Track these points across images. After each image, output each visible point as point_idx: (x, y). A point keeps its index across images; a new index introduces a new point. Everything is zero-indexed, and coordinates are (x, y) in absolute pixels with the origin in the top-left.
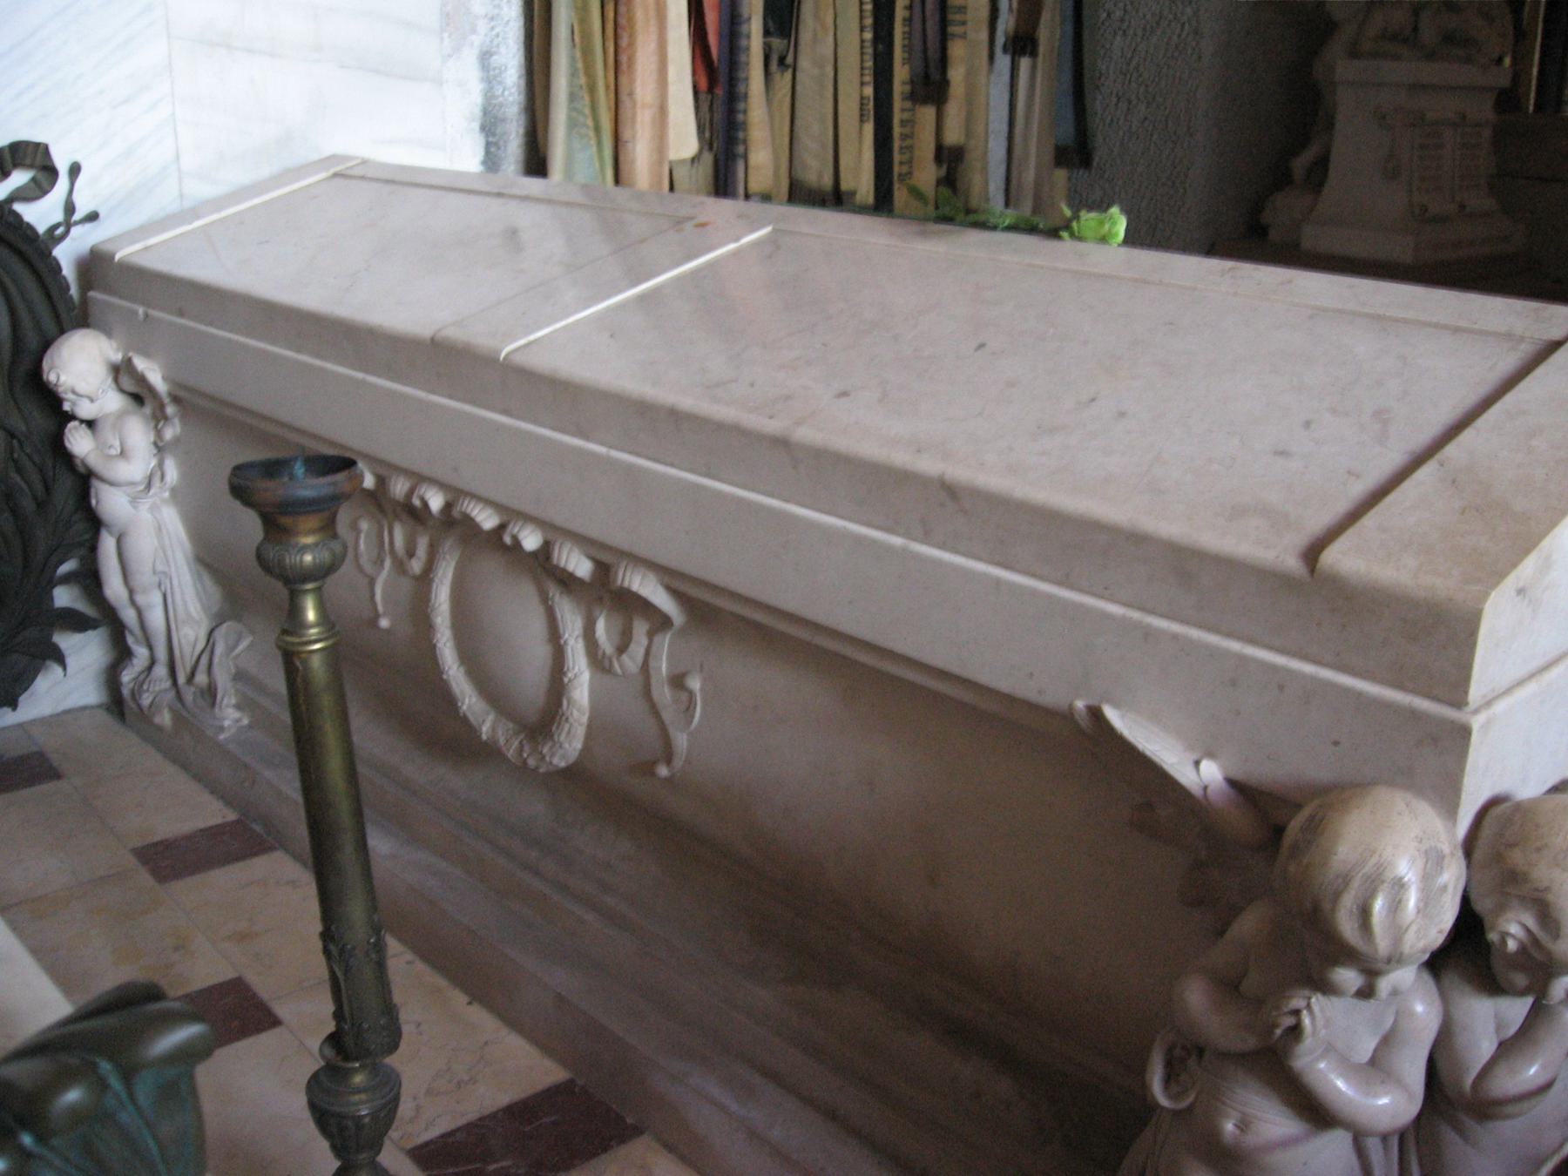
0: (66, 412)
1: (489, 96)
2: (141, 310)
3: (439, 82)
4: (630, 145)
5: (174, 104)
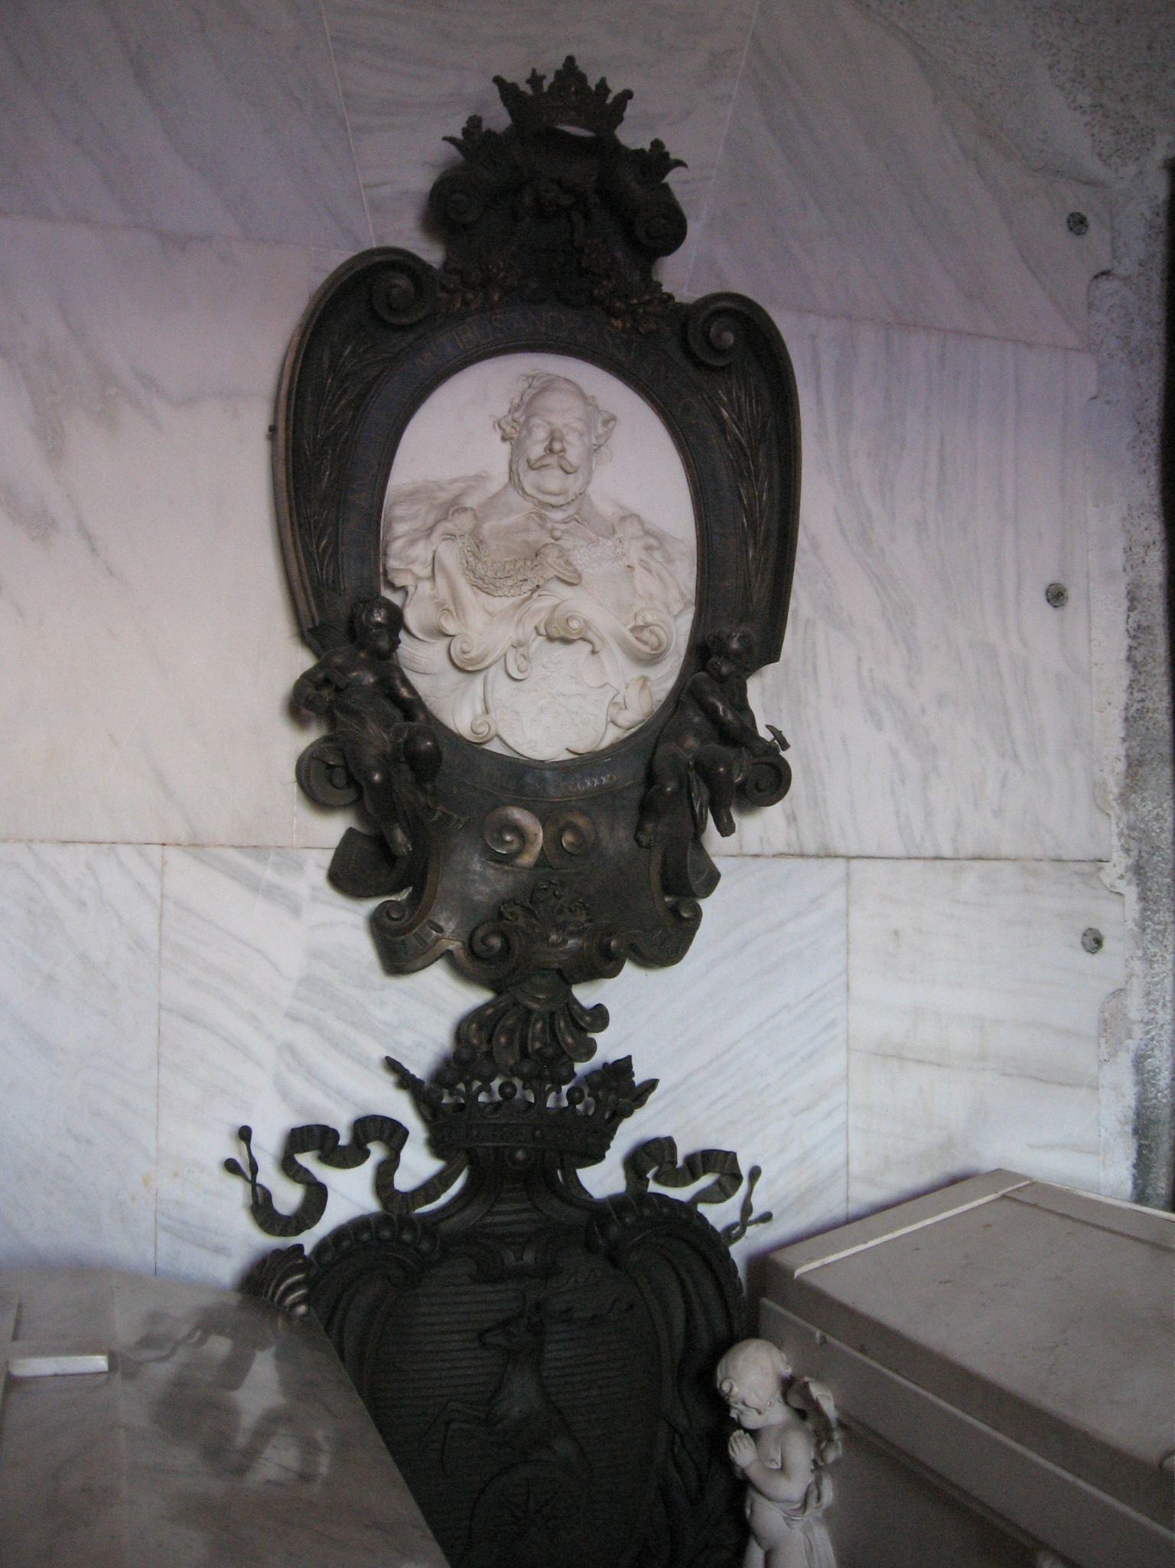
0: (733, 1419)
1: (1142, 1099)
2: (818, 1334)
3: (1095, 1087)
5: (847, 1112)
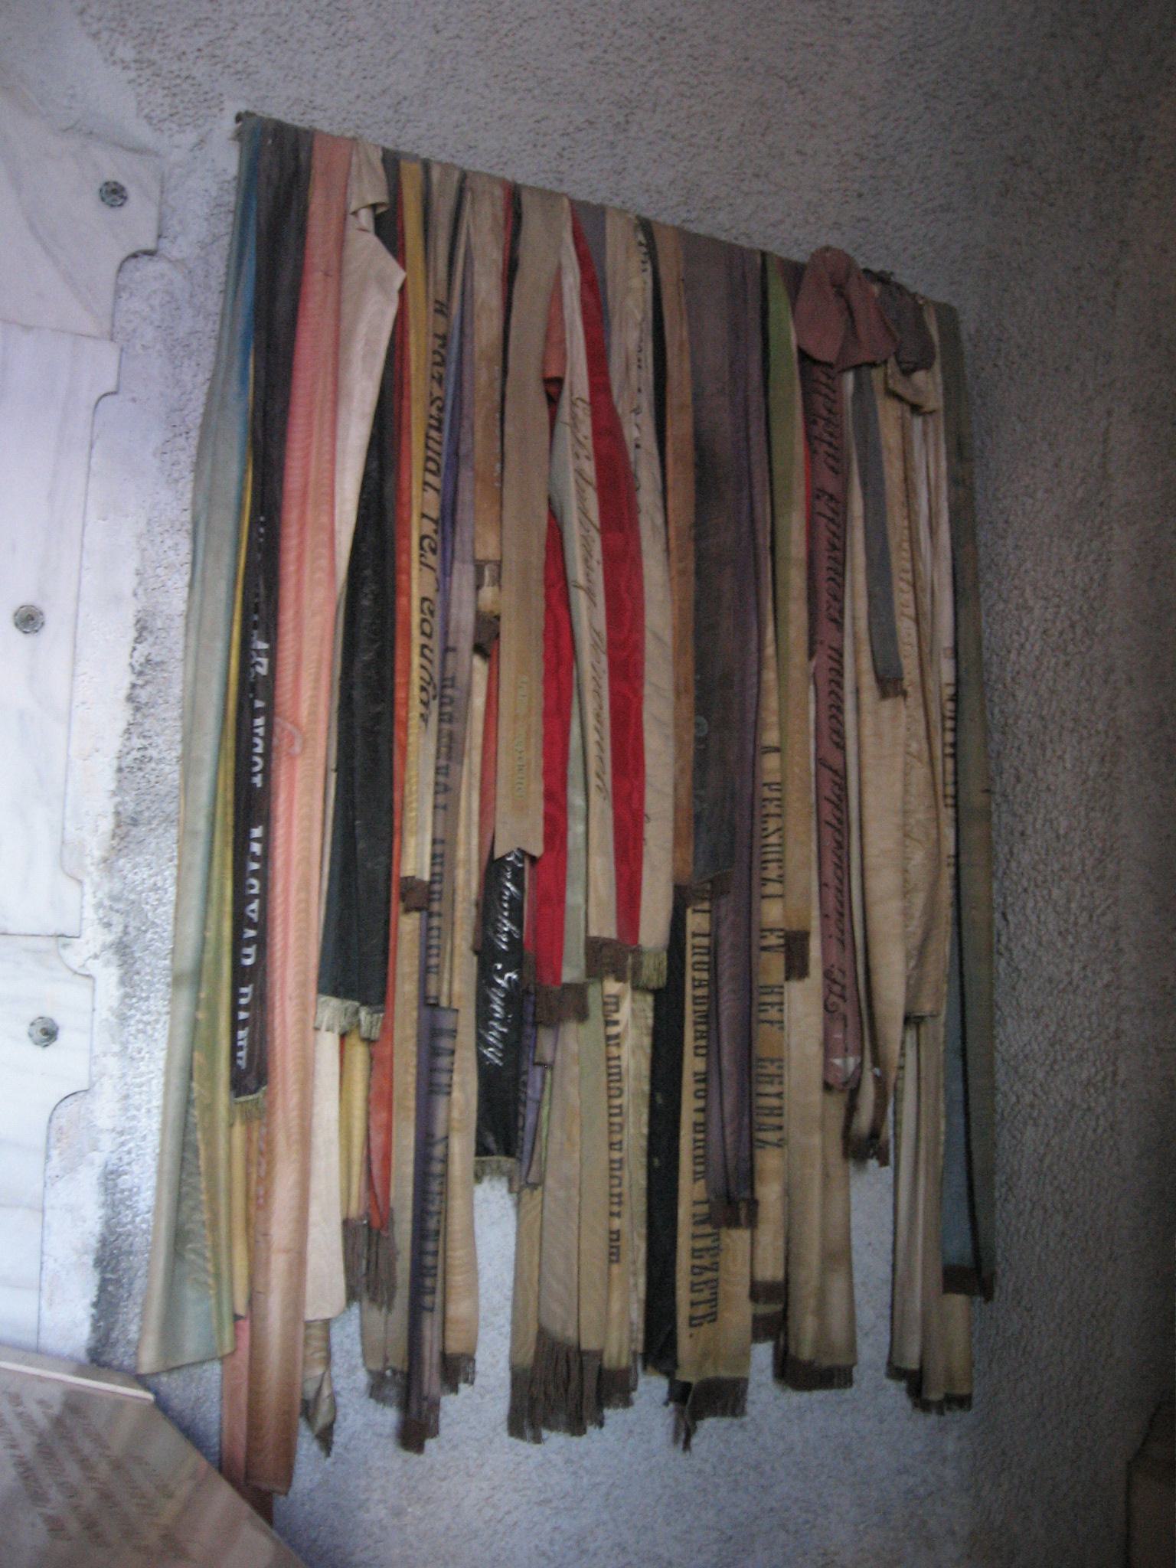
4: (262, 1297)
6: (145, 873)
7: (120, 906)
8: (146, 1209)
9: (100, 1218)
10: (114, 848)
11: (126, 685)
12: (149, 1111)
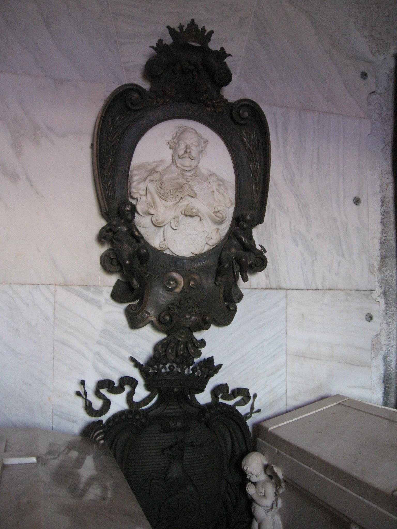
0: (248, 479)
1: (386, 371)
2: (276, 450)
3: (370, 367)
5: (286, 375)
6: (388, 272)
7: (384, 281)
8: (394, 367)
9: (383, 369)
10: (381, 265)
11: (380, 218)
12: (393, 339)
